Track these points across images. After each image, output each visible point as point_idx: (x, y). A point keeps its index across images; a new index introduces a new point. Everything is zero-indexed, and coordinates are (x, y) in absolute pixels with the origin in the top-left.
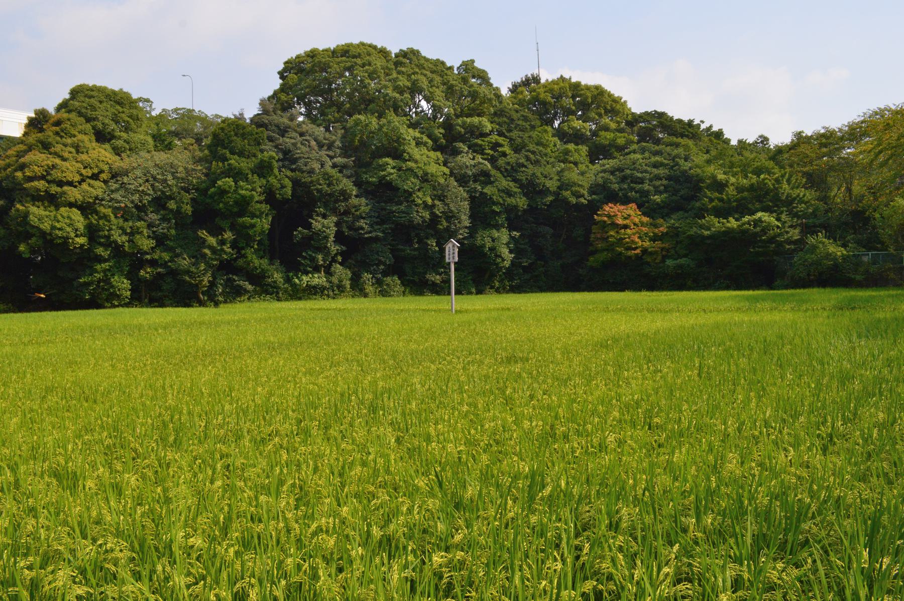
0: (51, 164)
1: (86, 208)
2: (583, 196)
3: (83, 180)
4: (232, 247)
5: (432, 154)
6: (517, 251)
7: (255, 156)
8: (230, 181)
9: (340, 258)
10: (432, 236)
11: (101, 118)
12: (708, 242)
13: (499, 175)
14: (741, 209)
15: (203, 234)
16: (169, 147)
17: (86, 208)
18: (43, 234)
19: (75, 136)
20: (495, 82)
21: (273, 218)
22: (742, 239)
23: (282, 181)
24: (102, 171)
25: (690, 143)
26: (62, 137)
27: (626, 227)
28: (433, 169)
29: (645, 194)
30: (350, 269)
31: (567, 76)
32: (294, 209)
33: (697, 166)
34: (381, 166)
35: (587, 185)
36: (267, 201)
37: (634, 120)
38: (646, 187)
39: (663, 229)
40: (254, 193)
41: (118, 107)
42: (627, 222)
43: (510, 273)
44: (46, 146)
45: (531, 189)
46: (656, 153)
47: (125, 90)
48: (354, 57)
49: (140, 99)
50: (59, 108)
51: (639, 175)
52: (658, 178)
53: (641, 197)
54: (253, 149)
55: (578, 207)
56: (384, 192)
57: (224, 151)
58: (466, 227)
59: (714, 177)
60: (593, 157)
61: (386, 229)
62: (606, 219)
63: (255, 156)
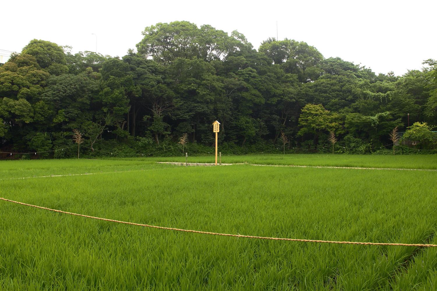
27: (316, 115)
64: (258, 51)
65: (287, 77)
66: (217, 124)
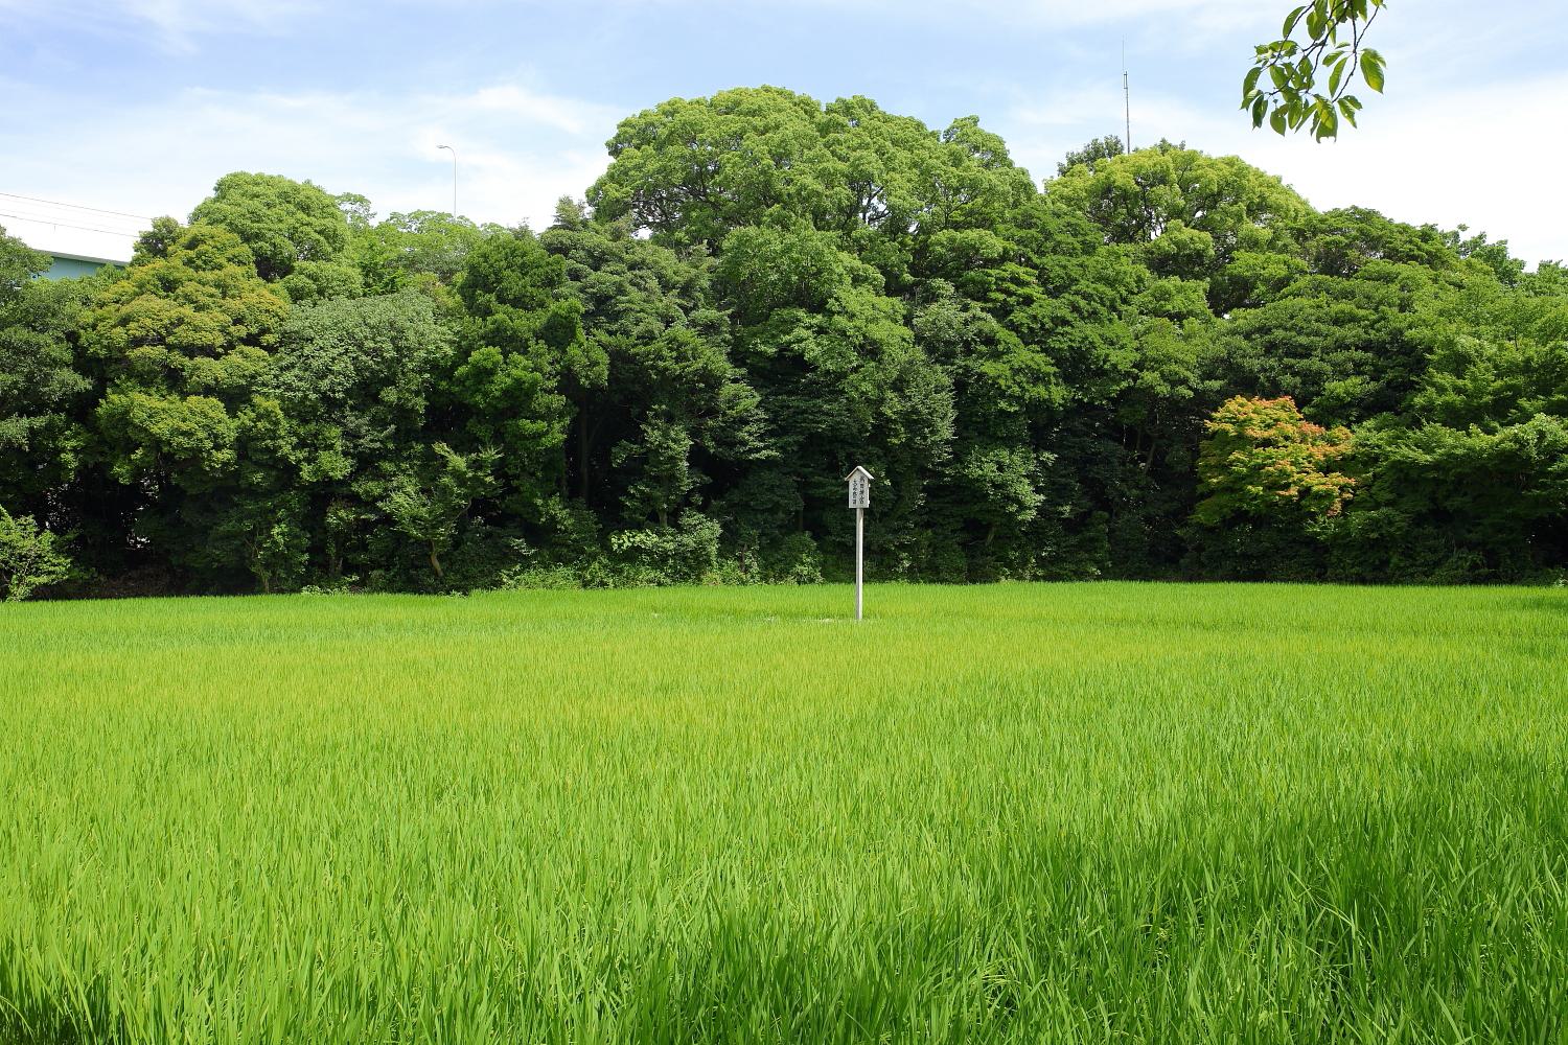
0: (174, 316)
1: (235, 397)
2: (1184, 381)
3: (230, 346)
4: (497, 474)
5: (885, 303)
6: (1054, 489)
7: (542, 305)
8: (495, 351)
9: (698, 499)
10: (879, 458)
11: (269, 234)
12: (1432, 475)
13: (1013, 339)
14: (1503, 409)
15: (441, 448)
16: (391, 287)
17: (235, 397)
18: (156, 443)
19: (220, 267)
20: (1019, 157)
21: (572, 421)
22: (1511, 468)
23: (590, 354)
24: (264, 331)
25: (1421, 272)
26: (197, 268)
27: (1266, 443)
28: (880, 331)
29: (1313, 379)
30: (718, 517)
31: (1175, 141)
32: (613, 407)
33: (1425, 323)
34: (785, 322)
35: (1192, 359)
36: (560, 390)
37: (1307, 229)
38: (1314, 363)
39: (1347, 448)
40: (538, 375)
41: (300, 215)
42: (1272, 432)
43: (1035, 533)
44: (169, 286)
45: (1076, 366)
46: (1347, 295)
47: (315, 183)
48: (753, 113)
49: (348, 198)
50: (195, 217)
51: (1303, 340)
52: (1341, 345)
53: (1303, 383)
54: (540, 294)
55: (1174, 403)
56: (781, 373)
57: (488, 296)
58: (947, 442)
59: (1450, 344)
60: (1219, 301)
61: (789, 444)
62: (1229, 427)
63: (542, 305)
64: (1041, 190)
65: (1164, 295)
66: (862, 479)
